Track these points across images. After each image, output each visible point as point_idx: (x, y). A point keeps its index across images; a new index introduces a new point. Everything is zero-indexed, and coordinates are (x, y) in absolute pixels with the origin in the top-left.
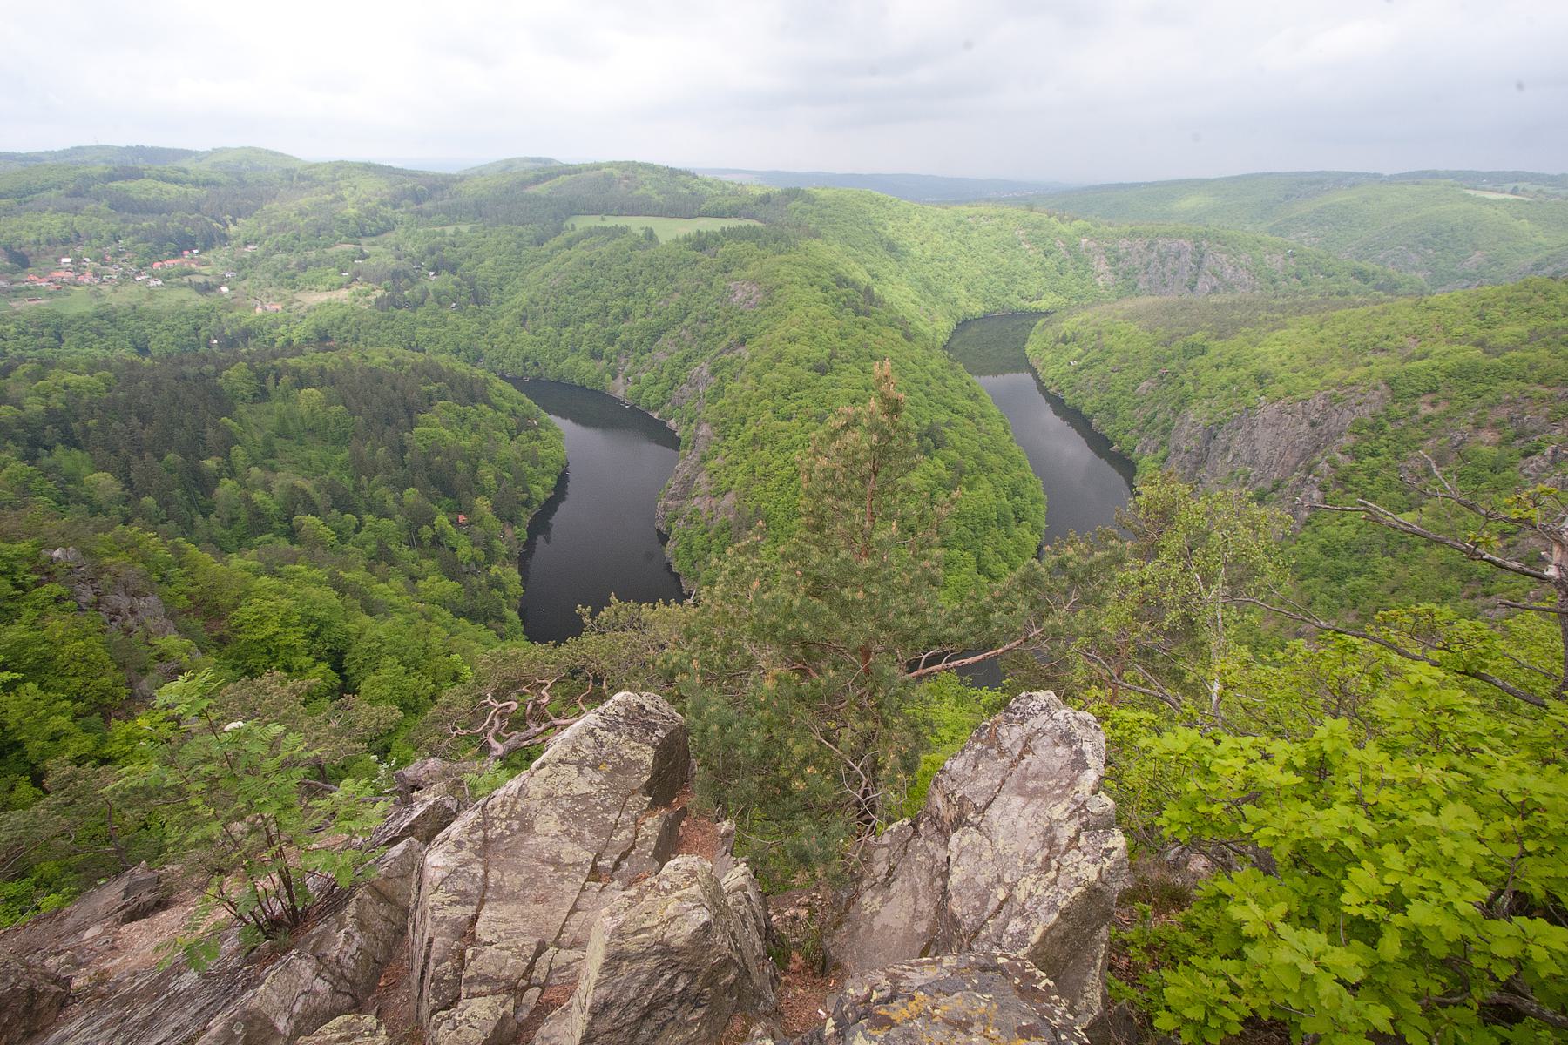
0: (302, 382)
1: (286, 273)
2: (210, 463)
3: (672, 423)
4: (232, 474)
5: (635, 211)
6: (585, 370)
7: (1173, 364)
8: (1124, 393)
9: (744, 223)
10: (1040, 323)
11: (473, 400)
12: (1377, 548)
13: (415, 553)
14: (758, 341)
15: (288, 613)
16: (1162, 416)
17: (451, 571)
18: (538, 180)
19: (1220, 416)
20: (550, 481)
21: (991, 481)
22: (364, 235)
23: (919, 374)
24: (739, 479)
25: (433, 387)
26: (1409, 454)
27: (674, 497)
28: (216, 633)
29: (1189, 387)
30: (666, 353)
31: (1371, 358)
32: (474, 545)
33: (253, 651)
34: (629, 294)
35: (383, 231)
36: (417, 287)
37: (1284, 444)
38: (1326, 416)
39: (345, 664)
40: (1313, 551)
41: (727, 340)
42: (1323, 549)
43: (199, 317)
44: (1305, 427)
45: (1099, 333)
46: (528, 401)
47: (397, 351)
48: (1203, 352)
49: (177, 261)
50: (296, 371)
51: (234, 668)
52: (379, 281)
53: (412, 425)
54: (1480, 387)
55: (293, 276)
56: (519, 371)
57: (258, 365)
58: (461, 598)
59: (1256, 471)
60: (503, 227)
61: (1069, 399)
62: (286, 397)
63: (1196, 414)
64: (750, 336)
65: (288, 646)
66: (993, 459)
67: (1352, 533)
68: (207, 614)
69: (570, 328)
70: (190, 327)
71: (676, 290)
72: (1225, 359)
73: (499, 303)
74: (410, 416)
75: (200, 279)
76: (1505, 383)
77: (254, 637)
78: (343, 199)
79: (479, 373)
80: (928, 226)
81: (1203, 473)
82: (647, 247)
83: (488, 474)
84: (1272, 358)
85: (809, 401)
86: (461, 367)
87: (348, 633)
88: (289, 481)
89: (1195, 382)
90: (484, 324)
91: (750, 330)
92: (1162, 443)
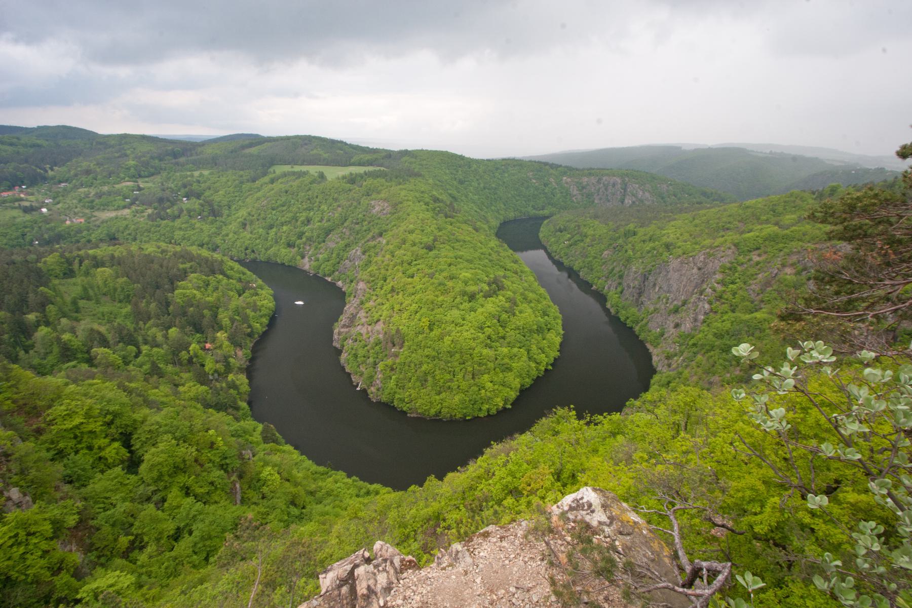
0: (98, 263)
1: (87, 199)
2: (32, 317)
3: (340, 284)
4: (47, 324)
5: (312, 162)
6: (284, 254)
7: (620, 241)
8: (595, 258)
9: (378, 168)
10: (546, 222)
11: (213, 272)
12: (743, 332)
13: (177, 369)
14: (390, 233)
15: (90, 409)
16: (617, 269)
17: (202, 379)
18: (251, 145)
19: (649, 267)
20: (265, 321)
21: (532, 308)
22: (140, 176)
23: (484, 250)
24: (385, 313)
25: (188, 265)
26: (751, 282)
27: (344, 326)
28: (34, 427)
29: (630, 252)
30: (334, 242)
31: (723, 233)
32: (217, 362)
33: (63, 437)
34: (310, 209)
35: (153, 175)
36: (175, 207)
37: (685, 280)
38: (705, 264)
39: (132, 442)
40: (710, 336)
41: (371, 234)
42: (715, 335)
43: (25, 227)
44: (695, 271)
45: (579, 226)
46: (249, 273)
47: (163, 245)
48: (635, 234)
49: (10, 193)
50: (94, 258)
51: (48, 450)
52: (150, 204)
53: (173, 290)
54: (781, 245)
55: (92, 201)
56: (242, 256)
57: (67, 255)
58: (209, 396)
59: (672, 295)
60: (230, 172)
61: (566, 262)
62: (87, 274)
63: (636, 267)
64: (385, 231)
65: (91, 432)
66: (531, 295)
67: (729, 325)
68: (28, 413)
69: (274, 230)
70: (19, 234)
71: (339, 206)
72: (647, 237)
73: (228, 216)
74: (172, 283)
75: (27, 204)
76: (793, 243)
77: (64, 427)
78: (126, 155)
79: (217, 256)
80: (480, 170)
81: (643, 299)
82: (320, 182)
83: (224, 317)
84: (672, 236)
85: (423, 266)
86: (205, 253)
87: (135, 421)
88: (89, 326)
89: (633, 250)
90: (220, 228)
91: (384, 227)
92: (620, 284)
